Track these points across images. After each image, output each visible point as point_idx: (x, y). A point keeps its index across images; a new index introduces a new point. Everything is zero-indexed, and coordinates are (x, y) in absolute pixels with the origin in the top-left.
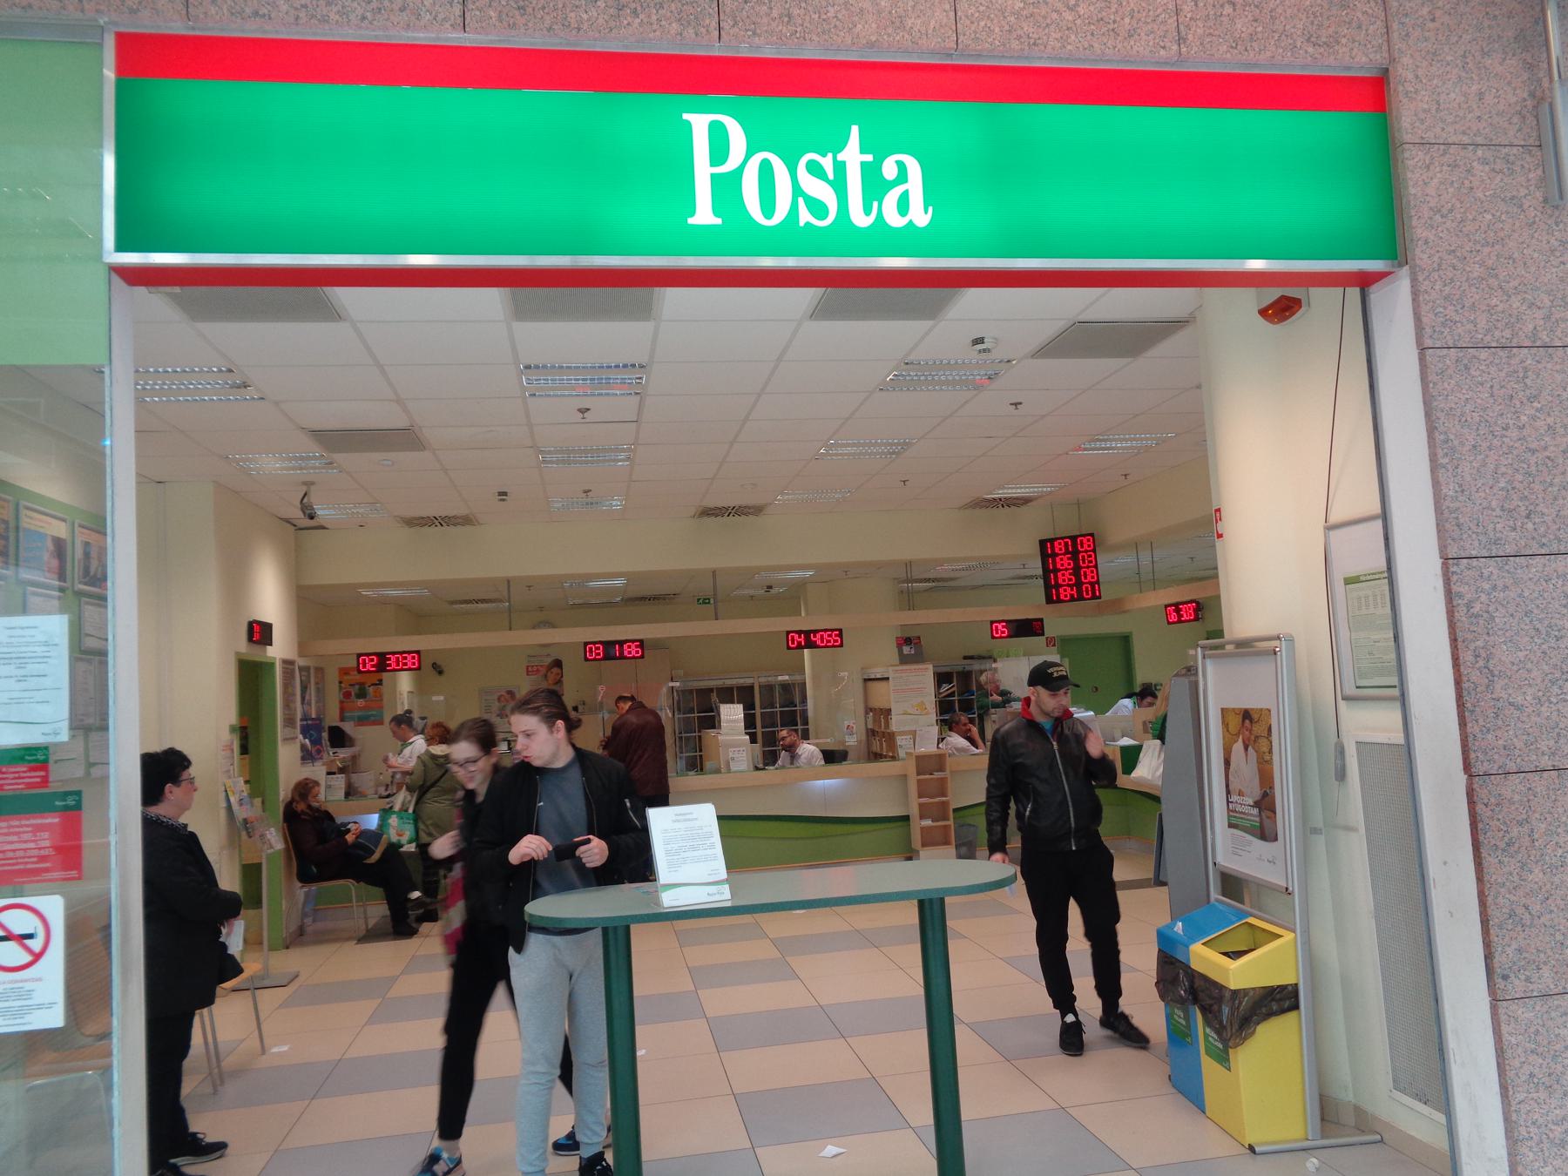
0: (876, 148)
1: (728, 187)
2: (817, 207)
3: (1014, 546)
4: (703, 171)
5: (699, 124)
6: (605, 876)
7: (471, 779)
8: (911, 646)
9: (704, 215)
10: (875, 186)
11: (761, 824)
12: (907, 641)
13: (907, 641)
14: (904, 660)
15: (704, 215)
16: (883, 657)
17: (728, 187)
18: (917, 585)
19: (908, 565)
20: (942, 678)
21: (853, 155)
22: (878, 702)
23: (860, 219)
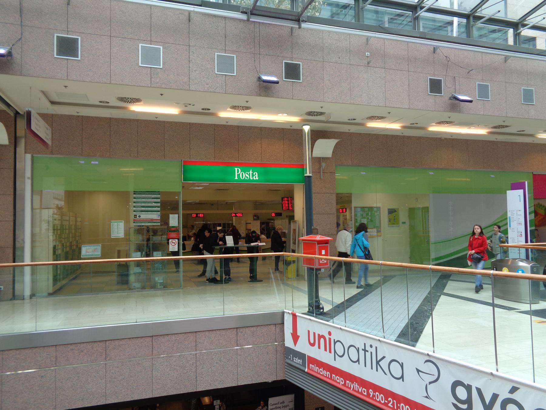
0: (253, 171)
1: (239, 175)
2: (247, 177)
3: (277, 198)
4: (236, 174)
5: (236, 169)
6: (68, 243)
7: (327, 301)
8: (256, 217)
9: (236, 178)
10: (253, 175)
11: (13, 162)
12: (255, 216)
13: (255, 216)
14: (254, 220)
15: (236, 178)
16: (250, 219)
17: (239, 175)
18: (257, 205)
19: (256, 201)
20: (262, 224)
21: (251, 172)
22: (248, 228)
23: (251, 179)
